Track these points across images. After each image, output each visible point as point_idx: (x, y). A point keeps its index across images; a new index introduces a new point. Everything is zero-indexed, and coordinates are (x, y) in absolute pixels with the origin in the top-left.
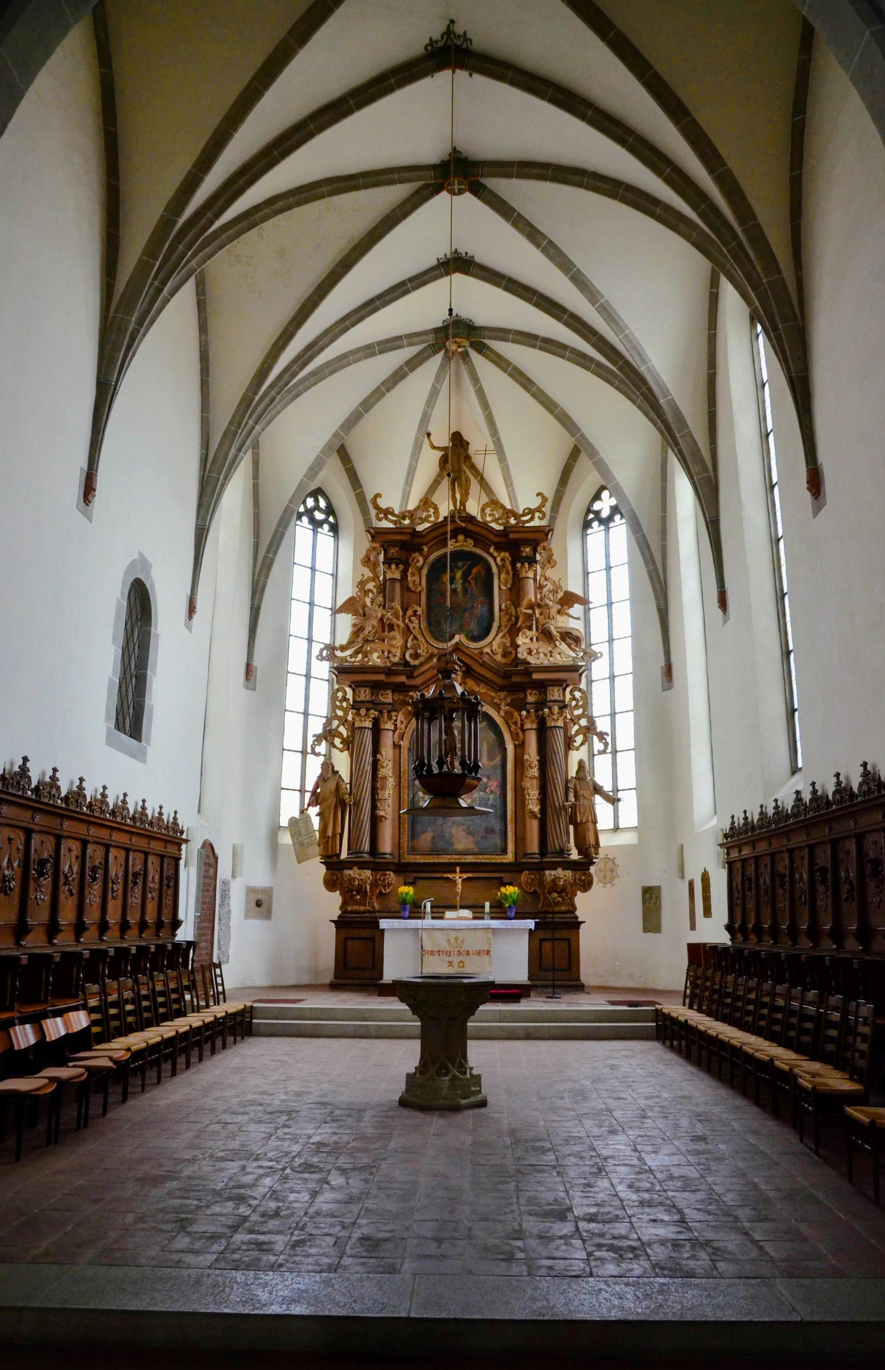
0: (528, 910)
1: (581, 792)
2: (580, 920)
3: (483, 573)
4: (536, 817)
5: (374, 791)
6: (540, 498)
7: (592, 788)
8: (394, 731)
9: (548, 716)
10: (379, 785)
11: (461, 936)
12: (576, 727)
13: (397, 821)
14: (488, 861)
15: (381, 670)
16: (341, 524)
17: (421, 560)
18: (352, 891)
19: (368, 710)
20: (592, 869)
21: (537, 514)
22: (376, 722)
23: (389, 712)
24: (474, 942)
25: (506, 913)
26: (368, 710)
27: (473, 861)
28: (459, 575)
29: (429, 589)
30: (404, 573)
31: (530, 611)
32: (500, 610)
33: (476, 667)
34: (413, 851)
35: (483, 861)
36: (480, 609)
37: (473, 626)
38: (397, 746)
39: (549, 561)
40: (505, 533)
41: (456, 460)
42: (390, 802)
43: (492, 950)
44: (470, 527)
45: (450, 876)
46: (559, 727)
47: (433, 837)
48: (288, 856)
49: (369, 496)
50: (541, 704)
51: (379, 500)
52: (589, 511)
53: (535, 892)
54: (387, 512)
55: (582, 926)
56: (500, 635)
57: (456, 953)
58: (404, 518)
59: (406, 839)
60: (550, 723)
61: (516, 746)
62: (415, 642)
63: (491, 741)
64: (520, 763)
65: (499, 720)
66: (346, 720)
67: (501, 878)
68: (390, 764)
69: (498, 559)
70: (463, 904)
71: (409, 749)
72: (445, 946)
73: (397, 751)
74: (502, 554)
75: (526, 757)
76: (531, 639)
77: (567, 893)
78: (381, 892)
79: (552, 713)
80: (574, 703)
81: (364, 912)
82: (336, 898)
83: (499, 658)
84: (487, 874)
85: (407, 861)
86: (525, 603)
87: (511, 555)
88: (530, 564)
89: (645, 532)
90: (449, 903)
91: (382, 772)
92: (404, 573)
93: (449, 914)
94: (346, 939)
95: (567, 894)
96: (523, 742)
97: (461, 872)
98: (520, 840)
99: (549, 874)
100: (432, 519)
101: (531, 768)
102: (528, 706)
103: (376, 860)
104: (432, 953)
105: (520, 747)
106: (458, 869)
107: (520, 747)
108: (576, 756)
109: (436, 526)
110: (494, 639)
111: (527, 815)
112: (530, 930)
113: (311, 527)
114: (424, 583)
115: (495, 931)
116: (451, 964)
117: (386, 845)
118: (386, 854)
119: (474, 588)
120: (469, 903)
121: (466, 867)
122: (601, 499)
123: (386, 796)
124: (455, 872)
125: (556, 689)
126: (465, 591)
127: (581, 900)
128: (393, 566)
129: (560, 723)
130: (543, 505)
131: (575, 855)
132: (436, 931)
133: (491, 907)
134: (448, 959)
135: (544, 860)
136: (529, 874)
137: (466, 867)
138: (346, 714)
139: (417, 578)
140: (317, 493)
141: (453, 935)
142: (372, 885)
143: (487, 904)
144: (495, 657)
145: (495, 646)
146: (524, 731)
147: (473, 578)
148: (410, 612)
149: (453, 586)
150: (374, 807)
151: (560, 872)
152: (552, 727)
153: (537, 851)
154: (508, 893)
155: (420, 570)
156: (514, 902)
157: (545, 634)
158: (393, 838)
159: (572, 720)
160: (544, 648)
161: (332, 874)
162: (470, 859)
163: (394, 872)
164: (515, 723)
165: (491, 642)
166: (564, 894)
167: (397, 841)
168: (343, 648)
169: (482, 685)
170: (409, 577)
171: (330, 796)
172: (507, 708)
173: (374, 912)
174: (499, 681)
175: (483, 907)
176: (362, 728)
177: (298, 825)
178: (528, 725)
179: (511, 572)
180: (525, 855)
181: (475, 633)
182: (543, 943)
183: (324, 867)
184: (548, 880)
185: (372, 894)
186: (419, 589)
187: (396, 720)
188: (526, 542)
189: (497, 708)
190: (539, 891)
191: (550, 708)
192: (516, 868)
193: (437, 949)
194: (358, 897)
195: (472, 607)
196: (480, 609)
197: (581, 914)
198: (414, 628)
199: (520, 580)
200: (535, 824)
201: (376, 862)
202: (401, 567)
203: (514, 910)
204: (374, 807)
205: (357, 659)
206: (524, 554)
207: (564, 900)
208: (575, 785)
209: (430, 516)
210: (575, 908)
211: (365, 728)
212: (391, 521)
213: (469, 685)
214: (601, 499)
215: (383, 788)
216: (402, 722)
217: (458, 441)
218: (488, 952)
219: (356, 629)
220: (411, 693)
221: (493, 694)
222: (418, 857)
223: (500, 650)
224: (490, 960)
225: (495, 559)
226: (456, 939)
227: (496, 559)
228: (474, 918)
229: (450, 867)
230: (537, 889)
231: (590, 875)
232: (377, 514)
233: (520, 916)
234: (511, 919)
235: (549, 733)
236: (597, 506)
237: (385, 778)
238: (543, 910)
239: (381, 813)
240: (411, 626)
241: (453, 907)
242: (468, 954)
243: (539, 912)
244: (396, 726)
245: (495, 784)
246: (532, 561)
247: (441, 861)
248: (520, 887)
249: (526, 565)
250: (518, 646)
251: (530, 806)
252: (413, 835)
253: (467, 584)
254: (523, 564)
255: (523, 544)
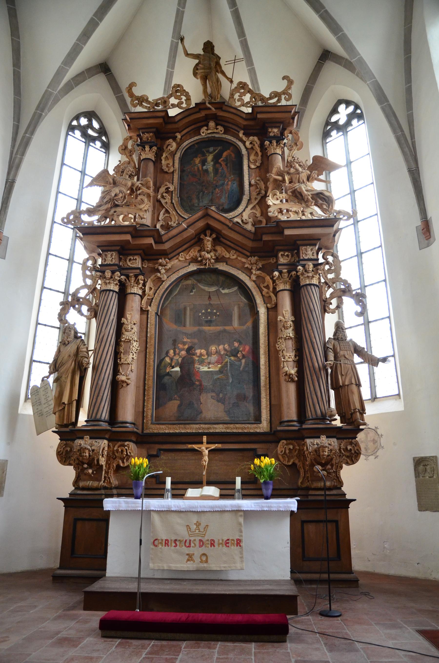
0: (286, 485)
1: (342, 353)
2: (348, 497)
3: (233, 155)
4: (292, 380)
5: (117, 354)
6: (286, 81)
7: (353, 350)
8: (142, 297)
9: (302, 274)
10: (122, 350)
11: (204, 520)
12: (331, 290)
13: (142, 388)
14: (240, 431)
15: (126, 230)
16: (112, 142)
17: (174, 145)
18: (83, 463)
19: (113, 272)
20: (360, 437)
21: (283, 97)
22: (123, 286)
23: (136, 276)
24: (218, 530)
25: (261, 489)
26: (113, 272)
27: (223, 431)
28: (210, 158)
29: (182, 171)
30: (158, 155)
31: (280, 178)
32: (250, 185)
33: (226, 232)
34: (158, 420)
35: (235, 431)
36: (231, 185)
37: (224, 200)
38: (143, 312)
39: (296, 144)
40: (251, 117)
41: (208, 64)
42: (134, 367)
43: (244, 539)
44: (221, 113)
45: (195, 447)
46: (314, 285)
47: (180, 406)
48: (27, 427)
49: (124, 86)
50: (292, 266)
51: (134, 90)
52: (328, 123)
53: (294, 464)
54: (142, 100)
55: (351, 505)
56: (250, 206)
57: (197, 543)
58: (157, 105)
59: (150, 406)
60: (304, 281)
61: (268, 309)
62: (166, 215)
63: (242, 305)
64: (273, 325)
65: (250, 284)
66: (95, 289)
67: (254, 450)
68: (136, 329)
69: (248, 144)
70: (212, 479)
71: (157, 314)
72: (183, 534)
73: (145, 316)
74: (251, 138)
75: (280, 318)
76: (281, 201)
77: (332, 465)
78: (118, 466)
79: (306, 271)
80: (327, 267)
81: (97, 489)
82: (70, 472)
83: (249, 227)
84: (239, 446)
85: (151, 431)
86: (274, 170)
87: (259, 139)
88: (278, 143)
89: (391, 102)
90: (196, 478)
91: (126, 336)
92: (158, 155)
93: (191, 492)
94: (76, 520)
95: (332, 465)
96: (276, 305)
97: (208, 443)
98: (275, 408)
99: (311, 443)
100: (184, 105)
101: (286, 328)
102: (280, 267)
103: (114, 429)
104: (167, 543)
105: (273, 310)
106: (205, 439)
107: (273, 310)
108: (330, 322)
109: (188, 112)
110: (244, 210)
111: (283, 378)
112: (292, 512)
113: (84, 140)
114: (177, 165)
115: (247, 514)
116: (190, 557)
117: (128, 413)
118: (126, 423)
119: (224, 169)
120: (218, 479)
121: (213, 437)
122: (338, 112)
123: (129, 360)
124: (202, 443)
125: (309, 248)
126: (216, 171)
127: (347, 473)
128: (147, 148)
129: (315, 281)
130: (289, 87)
131: (338, 423)
132: (173, 514)
133: (242, 483)
134: (186, 550)
135: (304, 426)
136: (287, 444)
137: (213, 437)
138: (95, 282)
139: (170, 162)
140: (90, 115)
141: (194, 519)
142: (109, 458)
143: (238, 480)
144: (245, 226)
145: (245, 216)
146: (276, 293)
147: (223, 160)
148: (162, 190)
149: (205, 167)
150: (116, 371)
151: (324, 440)
152: (307, 285)
153: (295, 418)
154: (263, 465)
155: (173, 154)
156: (271, 477)
157: (296, 196)
158: (136, 406)
159: (326, 283)
160: (295, 207)
161: (66, 445)
162: (220, 428)
163: (136, 443)
164: (267, 287)
165: (242, 213)
166: (329, 467)
167: (141, 410)
168: (90, 212)
169: (233, 252)
170: (163, 162)
171: (70, 363)
172: (258, 272)
173: (111, 489)
174: (250, 244)
175: (234, 483)
176: (107, 290)
177: (35, 395)
178: (281, 287)
179: (260, 154)
180: (281, 423)
181: (226, 207)
182: (305, 526)
183: (57, 437)
184: (310, 449)
185: (109, 468)
186: (171, 170)
187: (144, 285)
188: (274, 123)
189: (248, 272)
190: (299, 464)
191: (304, 266)
192: (271, 439)
193: (173, 538)
194: (90, 471)
195: (223, 184)
196: (231, 185)
197: (348, 490)
198: (166, 203)
199: (268, 157)
200: (292, 388)
201: (112, 429)
202: (154, 149)
203: (271, 487)
204: (116, 371)
205: (106, 223)
206: (272, 134)
207: (329, 473)
208: (334, 346)
209: (182, 103)
210: (341, 483)
211: (110, 290)
212: (146, 107)
213: (219, 252)
214: (338, 112)
215: (127, 352)
216: (151, 289)
217: (209, 47)
218: (239, 542)
219: (104, 194)
220: (160, 261)
221: (244, 260)
222: (162, 426)
223: (251, 220)
224: (241, 553)
225: (244, 143)
226: (198, 524)
227: (246, 144)
228: (222, 496)
229: (196, 438)
230: (297, 462)
231: (357, 444)
232: (132, 101)
233: (278, 494)
234: (267, 498)
235: (303, 291)
236: (334, 119)
237: (129, 341)
238: (304, 486)
239: (121, 378)
240: (163, 201)
241: (198, 484)
242: (212, 544)
243: (298, 489)
244: (144, 292)
245: (247, 348)
246: (279, 139)
247: (189, 431)
248: (277, 459)
249: (274, 142)
250: (269, 206)
251: (286, 369)
252: (159, 405)
253: (217, 165)
254: (271, 142)
255: (270, 123)
